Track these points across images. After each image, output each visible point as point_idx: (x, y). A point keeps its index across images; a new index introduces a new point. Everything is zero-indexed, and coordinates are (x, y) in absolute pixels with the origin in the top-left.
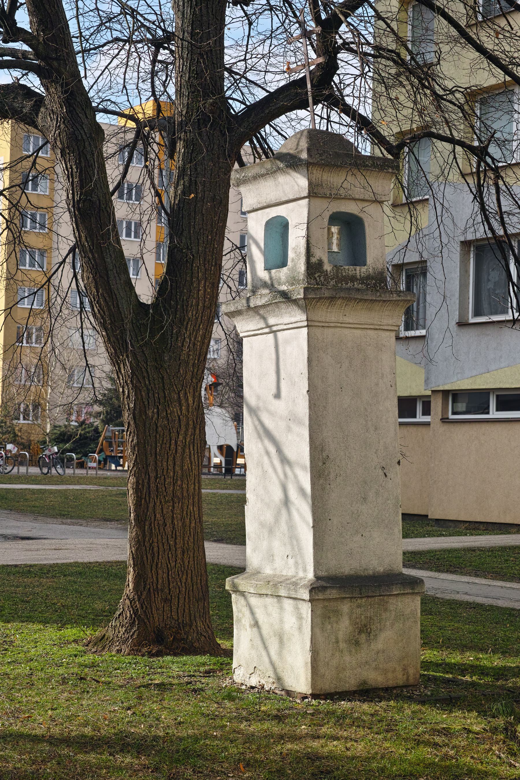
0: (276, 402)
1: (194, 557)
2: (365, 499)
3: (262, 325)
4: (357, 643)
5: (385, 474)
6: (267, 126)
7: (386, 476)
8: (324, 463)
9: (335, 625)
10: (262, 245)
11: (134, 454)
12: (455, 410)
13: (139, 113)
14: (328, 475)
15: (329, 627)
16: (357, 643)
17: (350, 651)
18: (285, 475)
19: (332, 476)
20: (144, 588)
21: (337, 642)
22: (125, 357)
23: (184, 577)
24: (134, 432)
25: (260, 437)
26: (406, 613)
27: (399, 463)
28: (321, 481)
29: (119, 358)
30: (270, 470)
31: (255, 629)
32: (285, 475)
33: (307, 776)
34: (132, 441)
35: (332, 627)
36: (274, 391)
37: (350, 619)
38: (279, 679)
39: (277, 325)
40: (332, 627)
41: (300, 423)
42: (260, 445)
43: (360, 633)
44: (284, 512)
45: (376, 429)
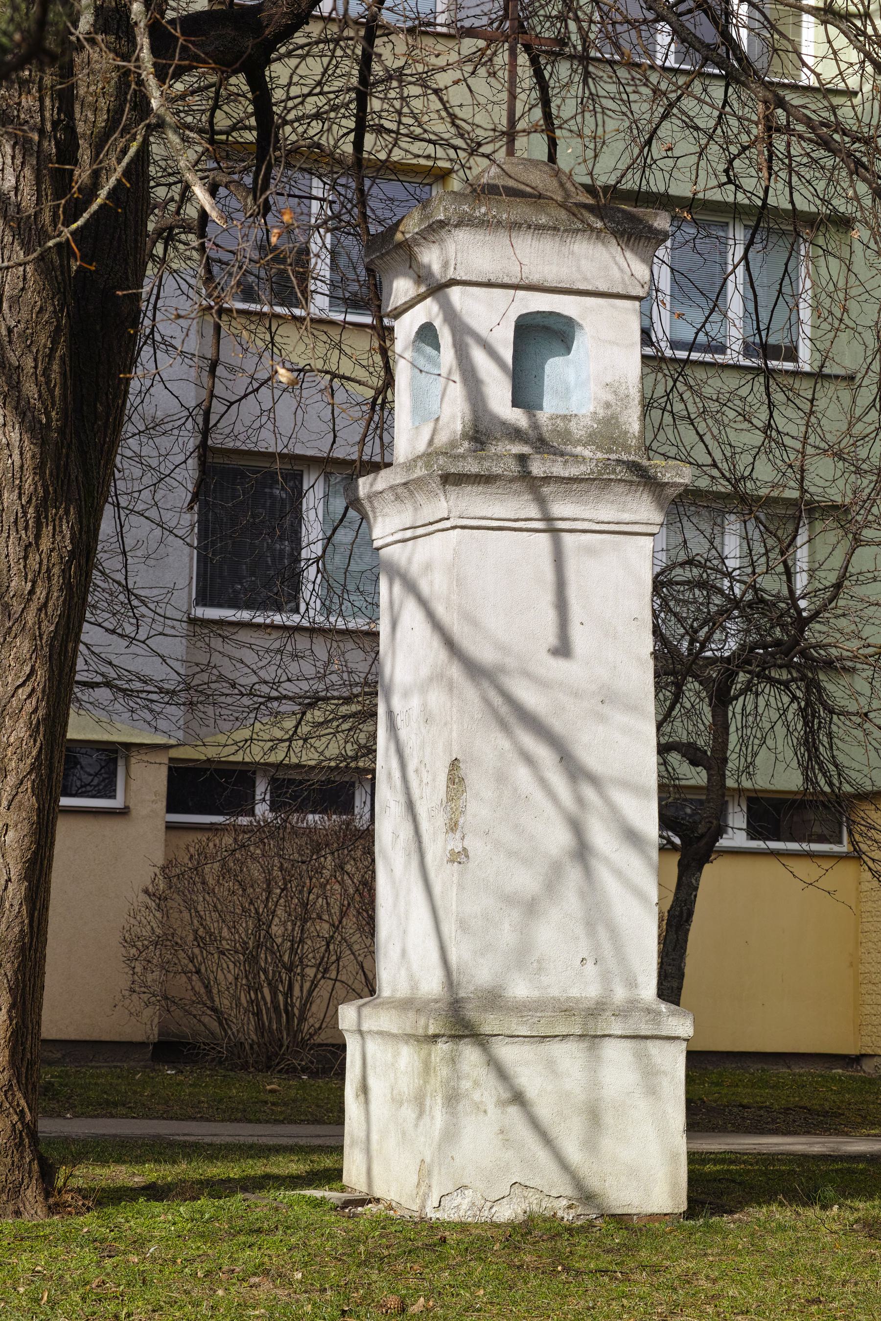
0: (559, 666)
3: (533, 511)
6: (275, 108)
10: (507, 354)
11: (35, 741)
12: (367, 643)
18: (580, 801)
20: (22, 1059)
22: (61, 512)
24: (43, 691)
25: (504, 726)
29: (47, 511)
30: (538, 796)
31: (513, 1111)
32: (580, 801)
33: (328, 1311)
34: (35, 711)
36: (551, 638)
38: (587, 1197)
39: (575, 520)
41: (633, 708)
42: (505, 744)
44: (573, 875)
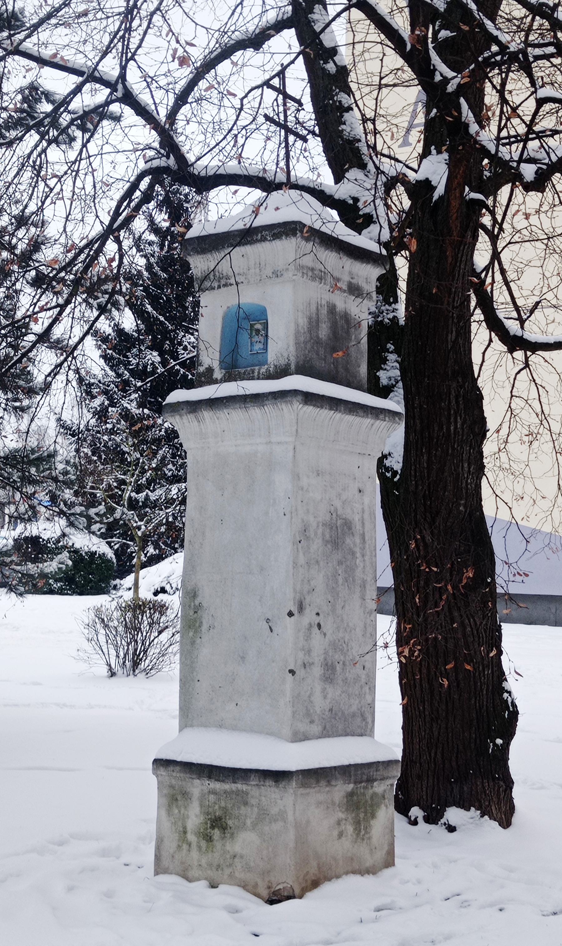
1: (447, 728)
2: (243, 658)
4: (209, 839)
5: (270, 627)
7: (272, 631)
8: (195, 612)
9: (183, 810)
13: (493, 213)
14: (200, 626)
15: (176, 811)
16: (209, 839)
17: (200, 848)
19: (205, 627)
21: (185, 832)
23: (433, 751)
26: (273, 812)
27: (318, 614)
28: (191, 634)
35: (180, 812)
37: (201, 806)
40: (180, 812)
43: (213, 827)
45: (262, 569)
